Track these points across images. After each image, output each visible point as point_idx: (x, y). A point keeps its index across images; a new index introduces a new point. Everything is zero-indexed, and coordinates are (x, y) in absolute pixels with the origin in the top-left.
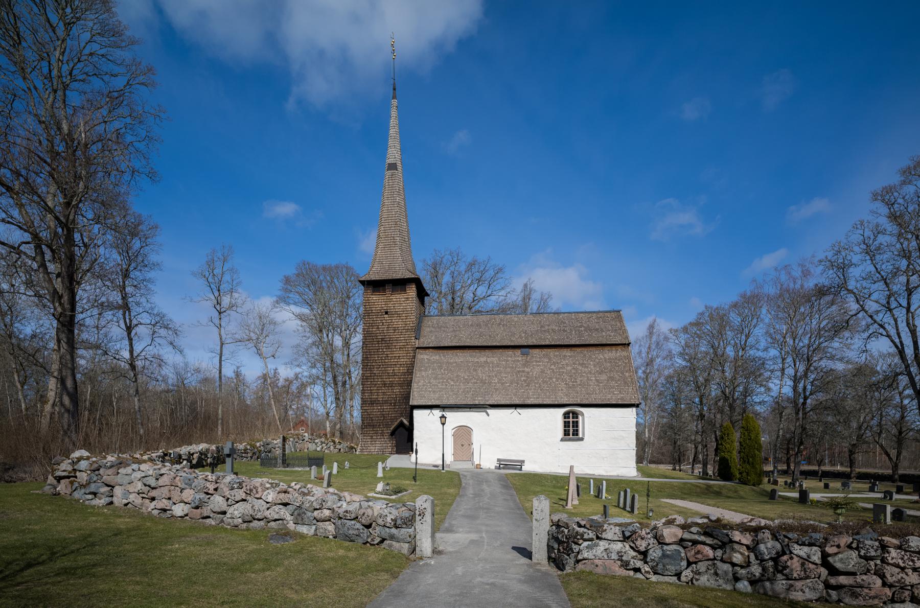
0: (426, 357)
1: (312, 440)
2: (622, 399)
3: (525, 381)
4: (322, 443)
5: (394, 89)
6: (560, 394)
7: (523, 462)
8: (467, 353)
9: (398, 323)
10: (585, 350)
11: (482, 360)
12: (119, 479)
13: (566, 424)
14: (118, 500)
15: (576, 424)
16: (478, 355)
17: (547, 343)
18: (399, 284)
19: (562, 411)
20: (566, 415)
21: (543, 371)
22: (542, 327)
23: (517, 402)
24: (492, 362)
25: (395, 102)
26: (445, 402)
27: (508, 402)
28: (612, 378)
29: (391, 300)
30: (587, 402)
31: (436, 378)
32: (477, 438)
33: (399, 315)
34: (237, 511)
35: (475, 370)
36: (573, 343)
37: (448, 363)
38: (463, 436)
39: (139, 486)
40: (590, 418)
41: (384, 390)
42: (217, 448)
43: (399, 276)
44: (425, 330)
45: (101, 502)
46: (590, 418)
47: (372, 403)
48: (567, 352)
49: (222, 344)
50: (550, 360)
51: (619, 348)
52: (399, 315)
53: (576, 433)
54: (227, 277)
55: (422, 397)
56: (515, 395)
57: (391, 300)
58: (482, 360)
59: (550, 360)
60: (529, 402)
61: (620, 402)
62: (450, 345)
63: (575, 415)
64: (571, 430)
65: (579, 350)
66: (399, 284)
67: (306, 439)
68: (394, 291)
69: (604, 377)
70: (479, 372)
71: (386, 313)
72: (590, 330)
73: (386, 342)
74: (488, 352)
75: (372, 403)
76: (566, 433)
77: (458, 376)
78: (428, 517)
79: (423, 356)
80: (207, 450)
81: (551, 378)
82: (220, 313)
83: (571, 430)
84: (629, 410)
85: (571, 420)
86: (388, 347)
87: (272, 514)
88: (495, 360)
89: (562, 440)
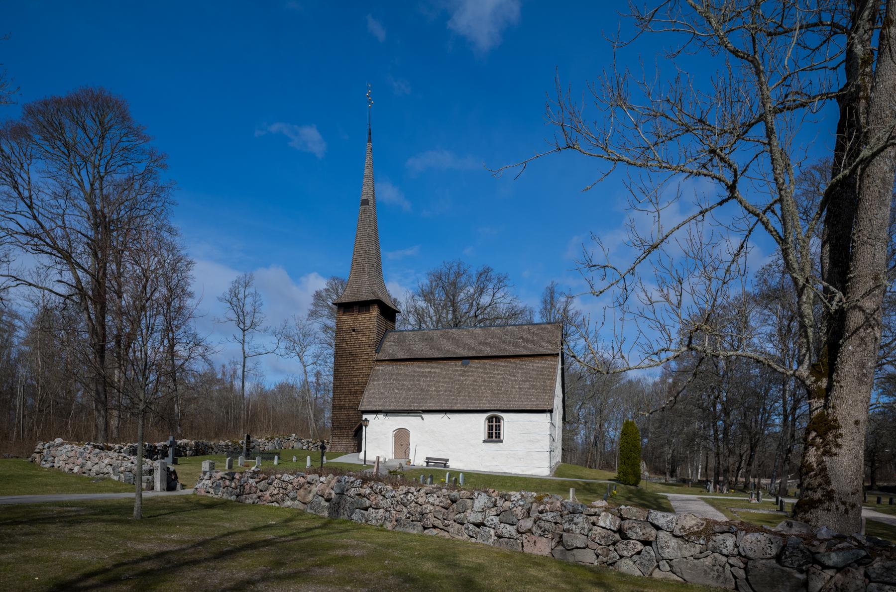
0: (381, 368)
1: (298, 440)
2: (537, 405)
3: (457, 389)
4: (308, 442)
5: (370, 134)
6: (484, 401)
7: (448, 460)
8: (410, 365)
9: (362, 339)
10: (518, 361)
11: (427, 370)
12: (57, 453)
13: (490, 428)
14: (56, 465)
15: (498, 428)
16: (425, 366)
17: (485, 354)
18: (364, 306)
19: (485, 416)
20: (490, 420)
21: (475, 381)
22: (486, 339)
23: (446, 408)
24: (435, 372)
25: (369, 145)
26: (387, 408)
27: (438, 408)
28: (533, 387)
29: (357, 319)
30: (505, 408)
31: (385, 387)
32: (414, 439)
33: (363, 332)
34: (95, 469)
35: (419, 380)
36: (507, 354)
37: (398, 373)
38: (402, 438)
39: (64, 457)
40: (509, 421)
41: (350, 397)
42: (196, 443)
43: (364, 298)
44: (387, 344)
45: (48, 466)
46: (509, 421)
47: (341, 408)
48: (502, 363)
49: (245, 357)
50: (485, 370)
51: (549, 359)
52: (363, 332)
53: (498, 436)
54: (249, 300)
55: (370, 403)
56: (446, 401)
57: (357, 319)
58: (427, 370)
59: (485, 370)
60: (455, 408)
61: (534, 408)
62: (403, 357)
63: (498, 420)
64: (494, 434)
65: (513, 360)
66: (364, 306)
67: (292, 439)
68: (360, 312)
69: (527, 385)
70: (422, 381)
71: (354, 331)
72: (527, 342)
73: (353, 356)
74: (434, 364)
75: (341, 408)
76: (490, 435)
77: (403, 385)
78: (159, 471)
79: (380, 368)
80: (187, 445)
81: (480, 387)
82: (244, 331)
83: (494, 434)
84: (544, 415)
85: (494, 424)
86: (354, 360)
87: (105, 471)
88: (438, 370)
89: (485, 442)
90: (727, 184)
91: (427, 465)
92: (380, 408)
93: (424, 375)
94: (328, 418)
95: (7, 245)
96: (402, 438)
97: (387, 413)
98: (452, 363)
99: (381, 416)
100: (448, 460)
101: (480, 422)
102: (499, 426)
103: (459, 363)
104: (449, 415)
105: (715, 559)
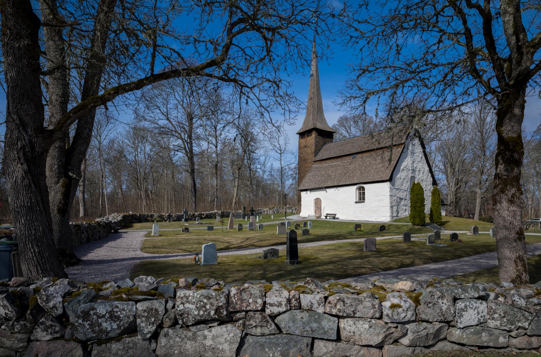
7: (335, 215)
8: (328, 161)
13: (360, 194)
15: (364, 193)
19: (356, 187)
20: (359, 189)
23: (336, 184)
38: (318, 202)
53: (364, 199)
60: (340, 184)
63: (363, 189)
64: (362, 198)
76: (360, 199)
83: (362, 198)
88: (339, 163)
89: (356, 202)
90: (363, 73)
91: (326, 218)
92: (307, 188)
93: (332, 166)
94: (440, 161)
95: (458, 25)
96: (318, 202)
97: (311, 190)
98: (348, 158)
99: (308, 192)
100: (335, 215)
101: (352, 191)
102: (364, 192)
103: (351, 157)
104: (339, 189)
105: (21, 275)
